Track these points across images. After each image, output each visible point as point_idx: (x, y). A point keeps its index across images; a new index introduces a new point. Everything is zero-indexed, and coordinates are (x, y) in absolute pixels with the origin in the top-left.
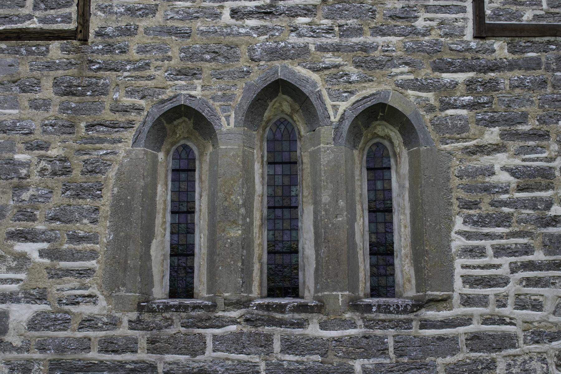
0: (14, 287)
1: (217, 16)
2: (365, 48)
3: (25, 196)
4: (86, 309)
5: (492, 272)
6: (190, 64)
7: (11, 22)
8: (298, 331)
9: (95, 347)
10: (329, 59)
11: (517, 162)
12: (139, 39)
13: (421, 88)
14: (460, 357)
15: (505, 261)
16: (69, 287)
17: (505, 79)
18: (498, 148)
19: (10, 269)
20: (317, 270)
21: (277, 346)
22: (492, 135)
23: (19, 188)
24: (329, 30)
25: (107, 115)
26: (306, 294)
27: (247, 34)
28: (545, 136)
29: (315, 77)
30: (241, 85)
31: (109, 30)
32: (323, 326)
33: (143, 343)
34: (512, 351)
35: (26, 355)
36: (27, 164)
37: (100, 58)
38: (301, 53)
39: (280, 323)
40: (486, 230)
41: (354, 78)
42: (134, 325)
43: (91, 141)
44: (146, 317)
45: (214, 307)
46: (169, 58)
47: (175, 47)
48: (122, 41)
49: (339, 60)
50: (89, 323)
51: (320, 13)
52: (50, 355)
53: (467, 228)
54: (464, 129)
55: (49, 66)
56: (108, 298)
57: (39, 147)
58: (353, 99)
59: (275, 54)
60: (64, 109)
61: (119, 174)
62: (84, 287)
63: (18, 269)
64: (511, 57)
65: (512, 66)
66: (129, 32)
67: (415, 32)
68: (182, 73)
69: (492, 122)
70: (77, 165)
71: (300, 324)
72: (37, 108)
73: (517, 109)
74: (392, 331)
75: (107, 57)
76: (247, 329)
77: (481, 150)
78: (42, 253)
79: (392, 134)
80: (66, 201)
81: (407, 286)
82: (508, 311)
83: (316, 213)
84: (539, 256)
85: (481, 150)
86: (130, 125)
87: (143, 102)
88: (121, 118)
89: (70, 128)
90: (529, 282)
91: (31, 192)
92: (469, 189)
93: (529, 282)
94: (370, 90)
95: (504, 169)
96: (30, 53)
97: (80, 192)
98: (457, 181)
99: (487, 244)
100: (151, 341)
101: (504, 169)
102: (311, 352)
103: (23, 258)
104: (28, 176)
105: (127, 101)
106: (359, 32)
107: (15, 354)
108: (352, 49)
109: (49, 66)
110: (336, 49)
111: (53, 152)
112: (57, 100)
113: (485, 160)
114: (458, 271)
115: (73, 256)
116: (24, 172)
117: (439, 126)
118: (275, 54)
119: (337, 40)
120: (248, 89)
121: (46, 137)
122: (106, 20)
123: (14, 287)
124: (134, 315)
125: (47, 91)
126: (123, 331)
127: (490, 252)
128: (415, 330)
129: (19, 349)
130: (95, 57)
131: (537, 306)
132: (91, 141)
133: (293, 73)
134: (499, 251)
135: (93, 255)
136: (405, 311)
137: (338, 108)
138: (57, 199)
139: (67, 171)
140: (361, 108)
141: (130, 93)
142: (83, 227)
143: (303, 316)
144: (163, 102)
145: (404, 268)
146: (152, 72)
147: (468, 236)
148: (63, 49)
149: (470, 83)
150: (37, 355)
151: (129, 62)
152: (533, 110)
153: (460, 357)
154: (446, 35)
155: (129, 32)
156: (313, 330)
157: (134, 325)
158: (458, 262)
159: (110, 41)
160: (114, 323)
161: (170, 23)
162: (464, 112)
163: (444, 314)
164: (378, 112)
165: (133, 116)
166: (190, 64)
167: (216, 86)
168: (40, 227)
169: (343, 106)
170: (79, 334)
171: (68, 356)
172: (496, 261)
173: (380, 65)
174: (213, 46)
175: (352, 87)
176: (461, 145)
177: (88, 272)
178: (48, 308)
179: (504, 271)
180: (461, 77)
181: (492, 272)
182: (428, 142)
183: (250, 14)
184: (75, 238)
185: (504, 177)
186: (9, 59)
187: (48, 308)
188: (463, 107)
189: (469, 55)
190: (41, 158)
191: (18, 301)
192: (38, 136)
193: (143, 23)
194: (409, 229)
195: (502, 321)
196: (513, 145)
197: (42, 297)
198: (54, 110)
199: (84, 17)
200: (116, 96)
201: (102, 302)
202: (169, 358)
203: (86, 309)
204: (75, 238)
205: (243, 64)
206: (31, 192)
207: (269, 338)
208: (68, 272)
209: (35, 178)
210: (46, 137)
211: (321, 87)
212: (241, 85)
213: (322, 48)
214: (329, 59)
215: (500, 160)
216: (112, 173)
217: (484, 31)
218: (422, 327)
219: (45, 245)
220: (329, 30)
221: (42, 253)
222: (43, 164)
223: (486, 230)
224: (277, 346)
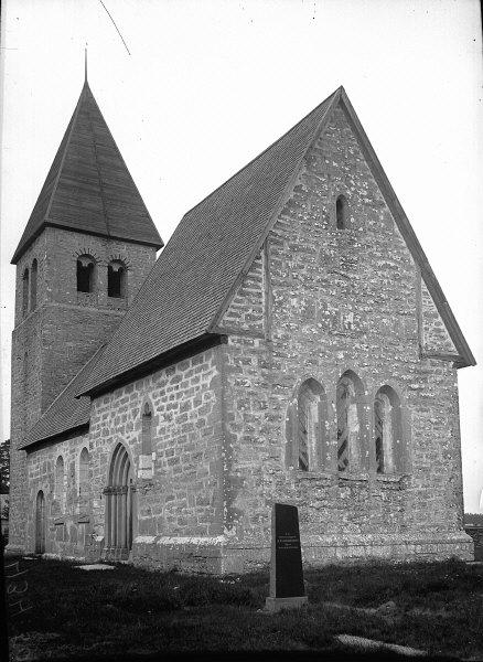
97: (272, 419)
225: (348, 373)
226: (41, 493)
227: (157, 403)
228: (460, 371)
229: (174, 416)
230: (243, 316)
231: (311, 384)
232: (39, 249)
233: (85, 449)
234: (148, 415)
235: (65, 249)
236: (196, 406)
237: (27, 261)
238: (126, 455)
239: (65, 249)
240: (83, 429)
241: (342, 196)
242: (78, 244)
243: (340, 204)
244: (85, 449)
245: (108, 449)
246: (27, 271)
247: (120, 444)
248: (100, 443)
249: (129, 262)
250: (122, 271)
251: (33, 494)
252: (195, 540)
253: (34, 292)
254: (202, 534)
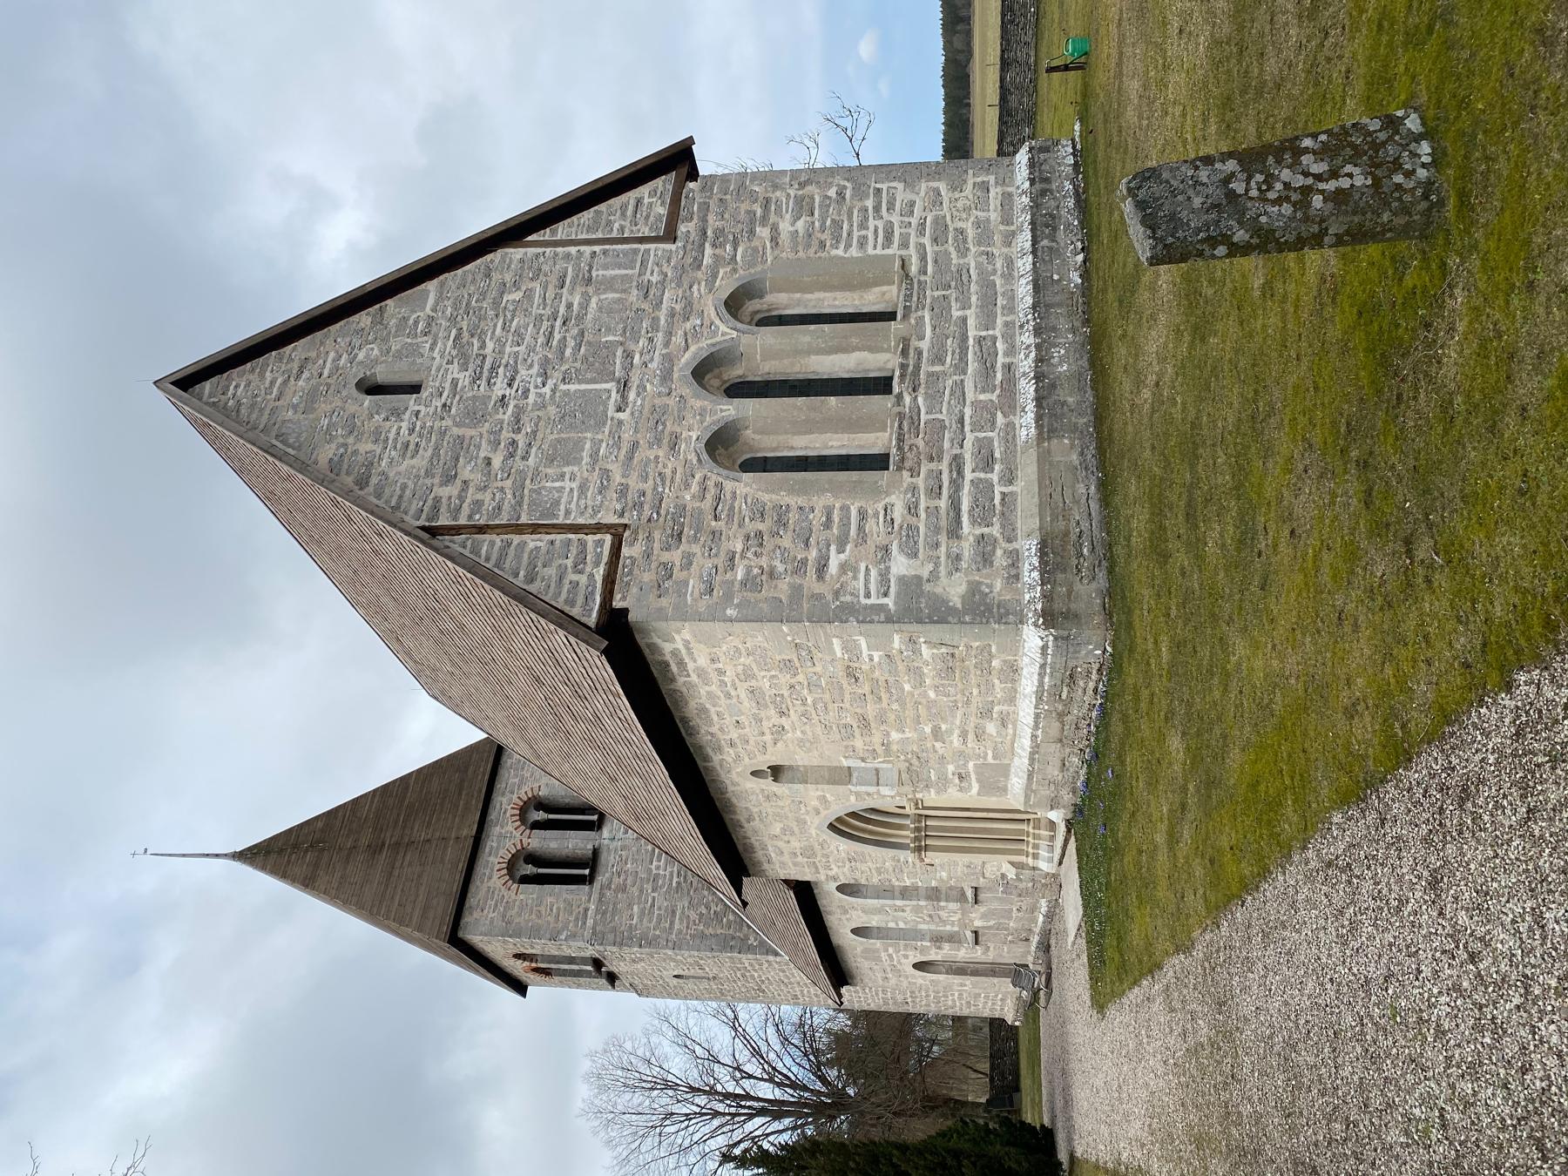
0: (874, 573)
1: (620, 422)
2: (672, 314)
3: (780, 568)
4: (898, 513)
5: (881, 232)
6: (665, 441)
7: (593, 593)
8: (925, 354)
9: (936, 502)
10: (678, 339)
11: (788, 216)
12: (634, 483)
13: (715, 276)
14: (952, 249)
15: (871, 223)
16: (875, 527)
17: (713, 222)
18: (775, 229)
19: (855, 578)
20: (872, 350)
21: (937, 368)
22: (763, 232)
23: (772, 574)
24: (651, 340)
25: (708, 504)
26: (890, 366)
27: (643, 399)
28: (768, 201)
29: (693, 349)
30: (692, 402)
31: (618, 507)
32: (922, 338)
33: (933, 466)
34: (948, 218)
35: (943, 559)
36: (749, 569)
37: (647, 512)
38: (669, 360)
39: (917, 367)
40: (845, 235)
41: (698, 322)
42: (914, 472)
43: (730, 517)
44: (908, 464)
45: (901, 416)
46: (657, 457)
47: (645, 453)
48: (632, 496)
49: (680, 332)
50: (912, 509)
51: (632, 347)
52: (943, 538)
53: (842, 246)
54: (755, 250)
55: (648, 555)
56: (888, 494)
57: (732, 559)
58: (718, 322)
59: (666, 376)
60: (696, 539)
61: (767, 491)
62: (876, 515)
63: (856, 570)
64: (695, 220)
65: (704, 220)
66: (623, 492)
67: (663, 282)
68: (673, 446)
69: (752, 232)
70: (752, 527)
71: (919, 353)
72: (690, 564)
73: (742, 216)
74: (928, 293)
75: (646, 507)
76: (922, 390)
77: (774, 240)
78: (840, 551)
79: (751, 309)
80: (790, 533)
81: (887, 297)
82: (914, 221)
83: (820, 352)
84: (870, 203)
85: (774, 240)
86: (720, 486)
87: (697, 477)
88: (712, 491)
89: (715, 535)
90: (891, 207)
91: (777, 563)
92: (809, 246)
93: (891, 207)
94: (711, 312)
95: (793, 224)
96: (630, 573)
97: (781, 522)
98: (801, 254)
99: (856, 234)
100: (931, 459)
101: (793, 224)
102: (943, 345)
103: (844, 567)
104: (761, 567)
105: (695, 488)
106: (656, 320)
107: (942, 568)
108: (670, 324)
109: (648, 555)
110: (669, 334)
111: (739, 547)
112: (684, 547)
113: (784, 237)
114: (879, 251)
115: (845, 524)
116: (756, 571)
117: (751, 264)
118: (666, 376)
119: (660, 335)
120: (697, 396)
121: (722, 554)
122: (608, 510)
123: (874, 573)
124: (906, 474)
125: (675, 556)
126: (920, 481)
127: (863, 232)
128: (925, 345)
129: (937, 565)
130: (644, 518)
131: (912, 204)
132: (730, 517)
133: (687, 364)
134: (863, 225)
135: (845, 509)
136: (912, 284)
137: (725, 331)
138: (786, 542)
139: (759, 534)
140: (728, 316)
141: (687, 486)
142: (817, 518)
143: (911, 351)
144: (699, 460)
145: (870, 300)
146: (668, 472)
147: (848, 246)
148: (632, 545)
149: (714, 246)
150: (943, 549)
151: (655, 489)
152: (744, 207)
153: (952, 249)
154: (669, 261)
155: (623, 492)
156: (925, 345)
157: (914, 472)
158: (870, 251)
159: (630, 504)
160: (914, 489)
161: (621, 457)
162: (740, 250)
163: (915, 260)
164: (733, 305)
165: (710, 483)
166: (665, 441)
167: (690, 420)
168: (813, 554)
169: (723, 328)
170: (923, 515)
171: (943, 523)
172: (872, 228)
173: (690, 304)
174: (652, 423)
175: (706, 323)
176: (769, 250)
177: (863, 515)
178: (895, 544)
179: (880, 224)
180: (708, 250)
181: (881, 232)
182: (764, 271)
183: (624, 397)
184: (828, 525)
185: (800, 224)
186: (634, 590)
187: (895, 544)
188: (735, 250)
189: (689, 247)
190: (743, 557)
191: (888, 569)
192: (720, 561)
193: (617, 478)
194: (838, 294)
195: (923, 225)
196: (773, 218)
197: (886, 550)
198: (696, 549)
199: (598, 528)
200: (688, 497)
201: (893, 499)
202: (946, 445)
203: (898, 513)
204: (828, 525)
205: (672, 402)
206: (777, 563)
207: (930, 374)
208: (860, 529)
209: (764, 562)
210: (722, 554)
211: (704, 344)
212: (692, 402)
213: (667, 344)
214: (678, 339)
215: (785, 227)
216: (765, 497)
217: (670, 235)
218: (925, 273)
219: (833, 548)
220: (651, 340)
221: (840, 551)
222: (749, 555)
223: (845, 235)
224: (937, 368)
225: (701, 372)
226: (919, 966)
227: (751, 756)
228: (703, 169)
229: (776, 720)
230: (575, 577)
231: (720, 444)
232: (497, 950)
233: (839, 888)
234: (776, 772)
235: (502, 911)
236: (753, 676)
237: (518, 968)
238: (853, 815)
239: (502, 911)
240: (805, 893)
241: (359, 385)
242: (491, 876)
243: (373, 389)
244: (839, 888)
245: (843, 845)
246: (536, 970)
247: (831, 827)
248: (832, 864)
249: (525, 792)
250: (541, 805)
251: (922, 978)
252: (1028, 683)
253: (571, 960)
254: (1013, 670)
